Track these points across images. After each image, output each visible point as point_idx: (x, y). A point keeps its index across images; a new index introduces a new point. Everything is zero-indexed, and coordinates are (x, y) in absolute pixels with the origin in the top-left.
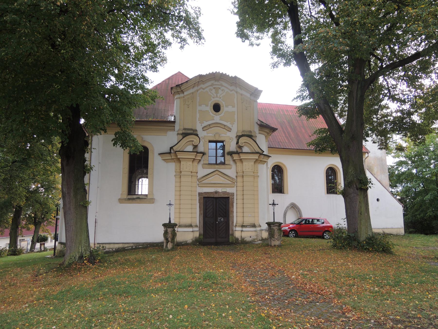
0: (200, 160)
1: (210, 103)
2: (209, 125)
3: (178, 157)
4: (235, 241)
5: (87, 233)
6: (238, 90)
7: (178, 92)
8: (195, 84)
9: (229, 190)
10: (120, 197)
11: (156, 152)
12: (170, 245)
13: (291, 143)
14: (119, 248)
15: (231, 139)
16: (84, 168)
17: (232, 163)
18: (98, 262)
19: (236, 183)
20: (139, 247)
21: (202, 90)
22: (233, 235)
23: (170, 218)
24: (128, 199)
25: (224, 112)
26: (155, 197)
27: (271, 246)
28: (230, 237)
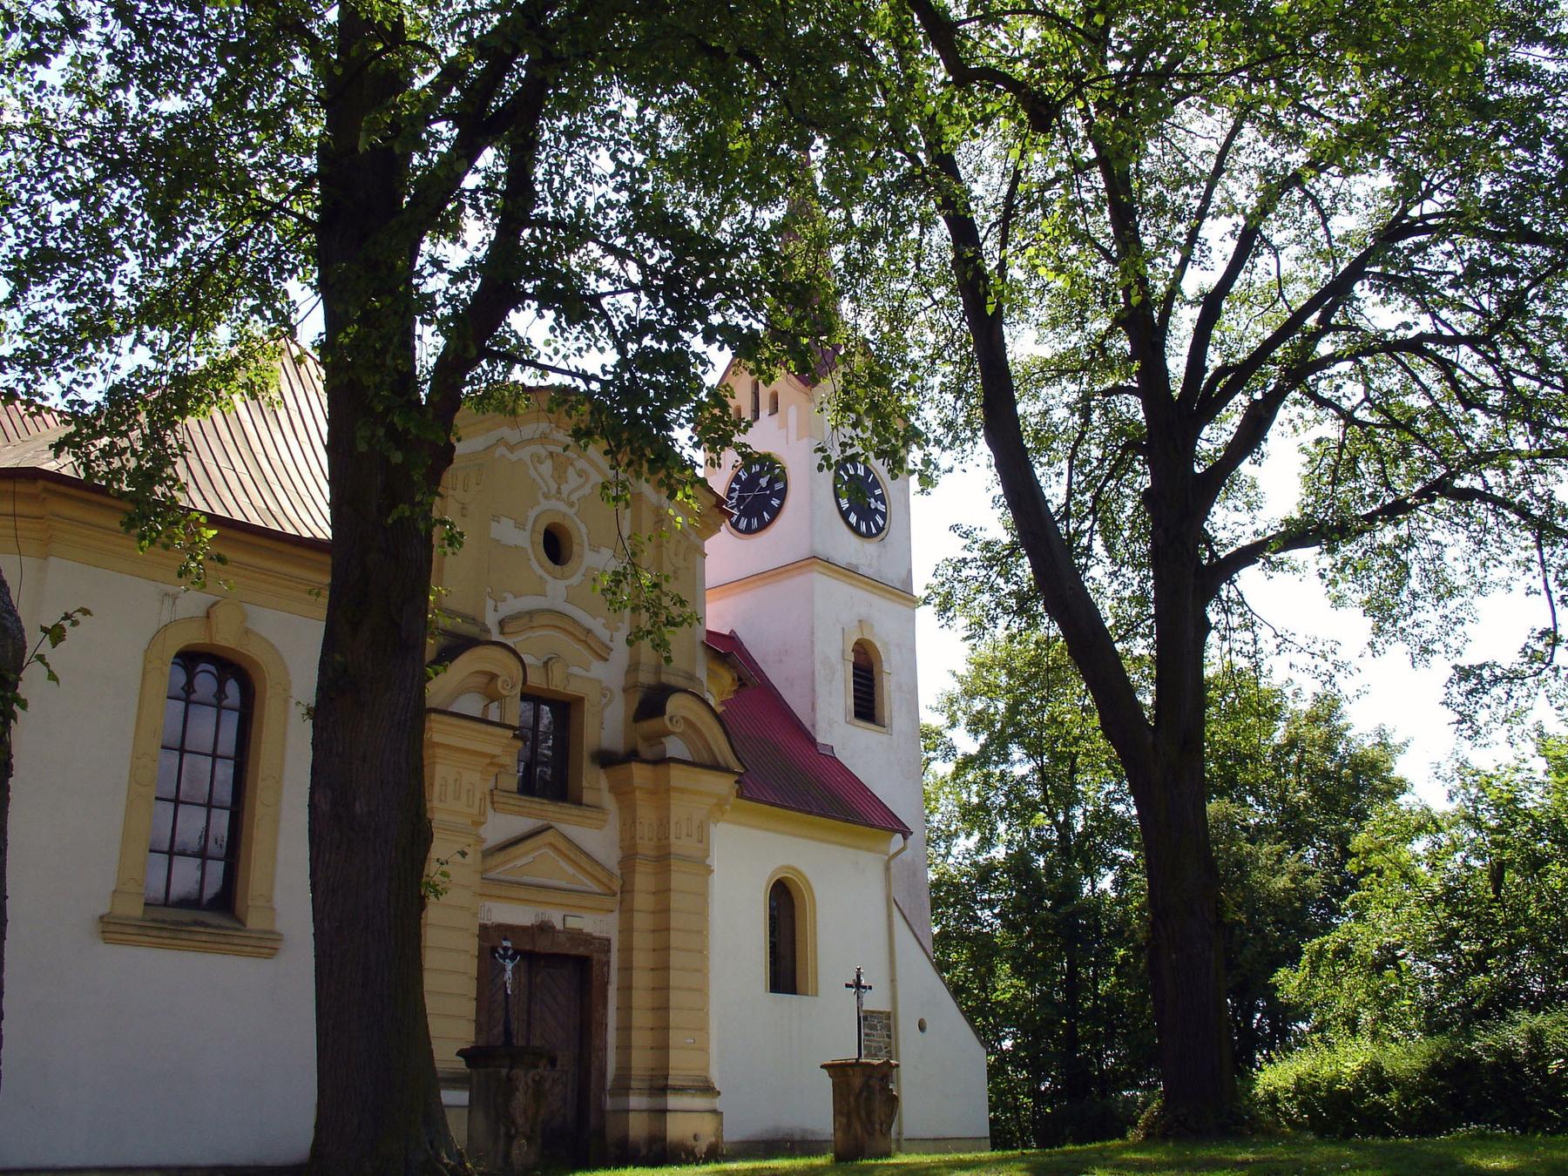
2: (531, 614)
15: (605, 692)
17: (609, 801)
21: (502, 450)
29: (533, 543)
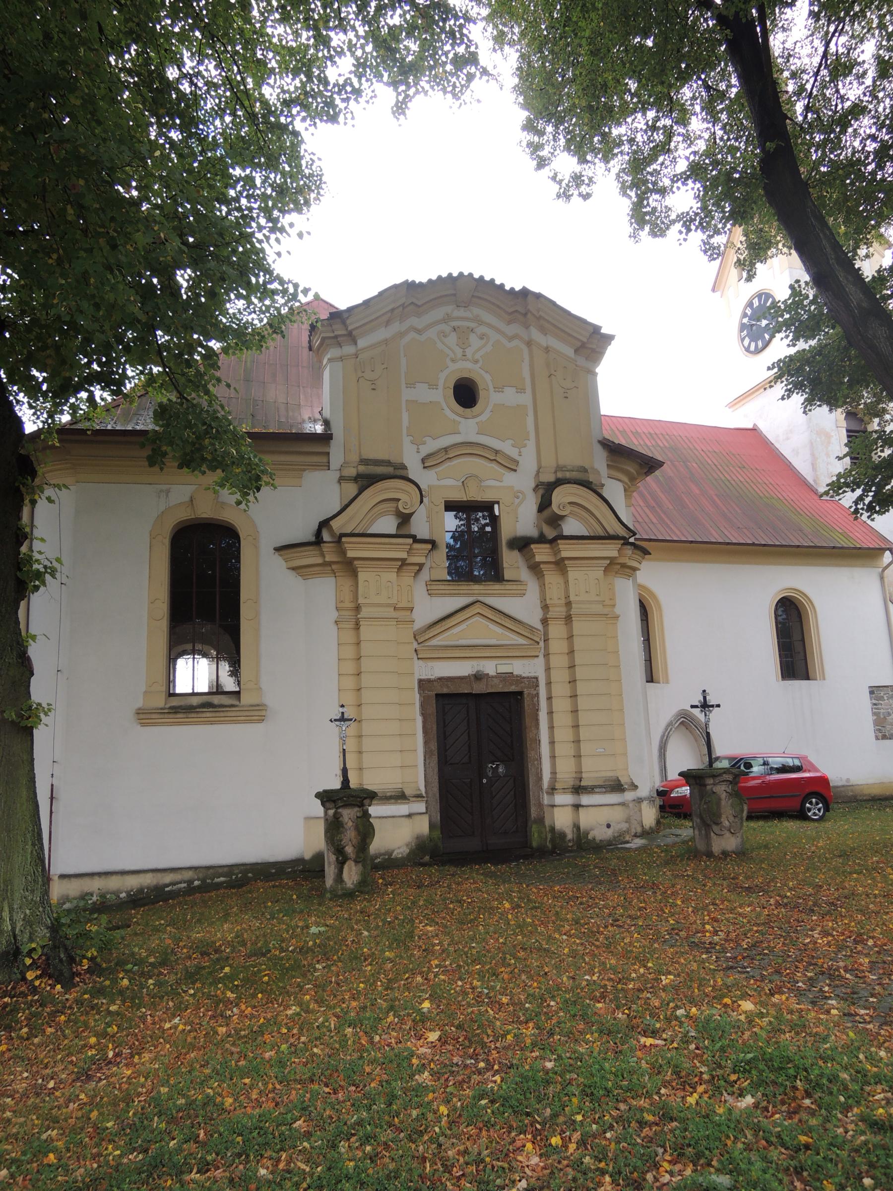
0: (421, 566)
1: (443, 376)
2: (446, 450)
3: (350, 554)
4: (552, 840)
5: (33, 845)
6: (536, 335)
7: (336, 337)
8: (393, 310)
9: (519, 668)
10: (140, 704)
11: (267, 544)
12: (353, 873)
13: (668, 526)
14: (140, 890)
15: (518, 495)
16: (20, 570)
17: (524, 574)
18: (89, 971)
19: (542, 644)
20: (216, 880)
21: (412, 335)
22: (541, 821)
23: (345, 771)
24: (171, 708)
25: (490, 408)
26: (269, 699)
27: (709, 854)
28: (534, 828)
29: (445, 397)
